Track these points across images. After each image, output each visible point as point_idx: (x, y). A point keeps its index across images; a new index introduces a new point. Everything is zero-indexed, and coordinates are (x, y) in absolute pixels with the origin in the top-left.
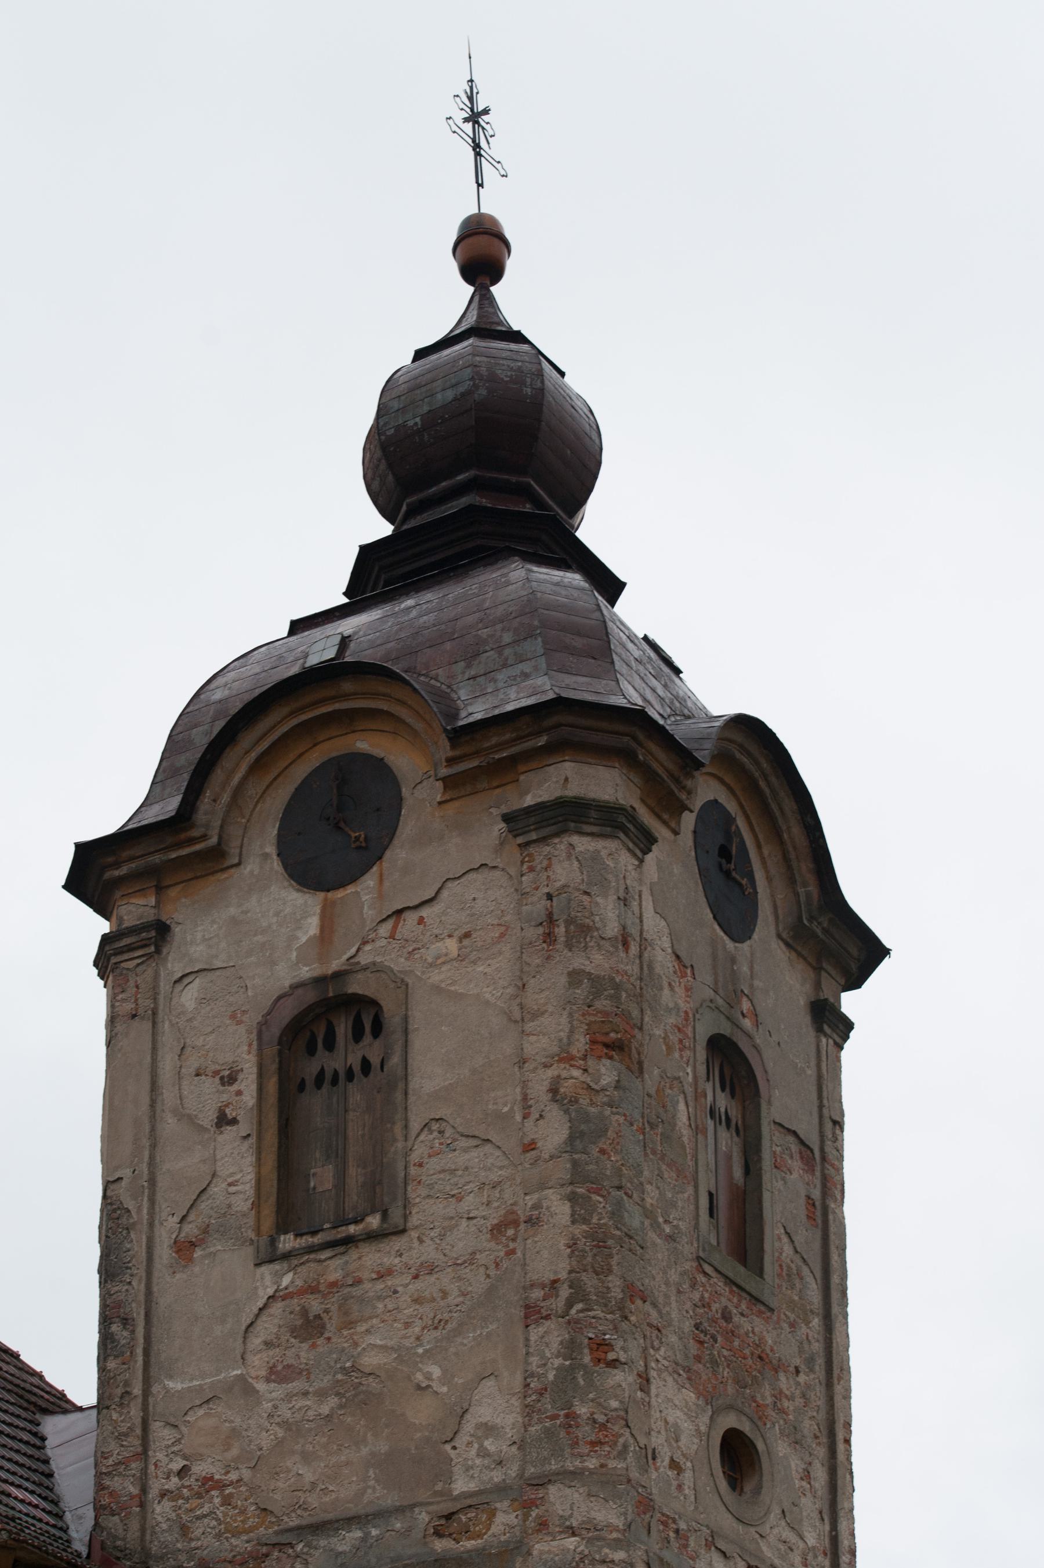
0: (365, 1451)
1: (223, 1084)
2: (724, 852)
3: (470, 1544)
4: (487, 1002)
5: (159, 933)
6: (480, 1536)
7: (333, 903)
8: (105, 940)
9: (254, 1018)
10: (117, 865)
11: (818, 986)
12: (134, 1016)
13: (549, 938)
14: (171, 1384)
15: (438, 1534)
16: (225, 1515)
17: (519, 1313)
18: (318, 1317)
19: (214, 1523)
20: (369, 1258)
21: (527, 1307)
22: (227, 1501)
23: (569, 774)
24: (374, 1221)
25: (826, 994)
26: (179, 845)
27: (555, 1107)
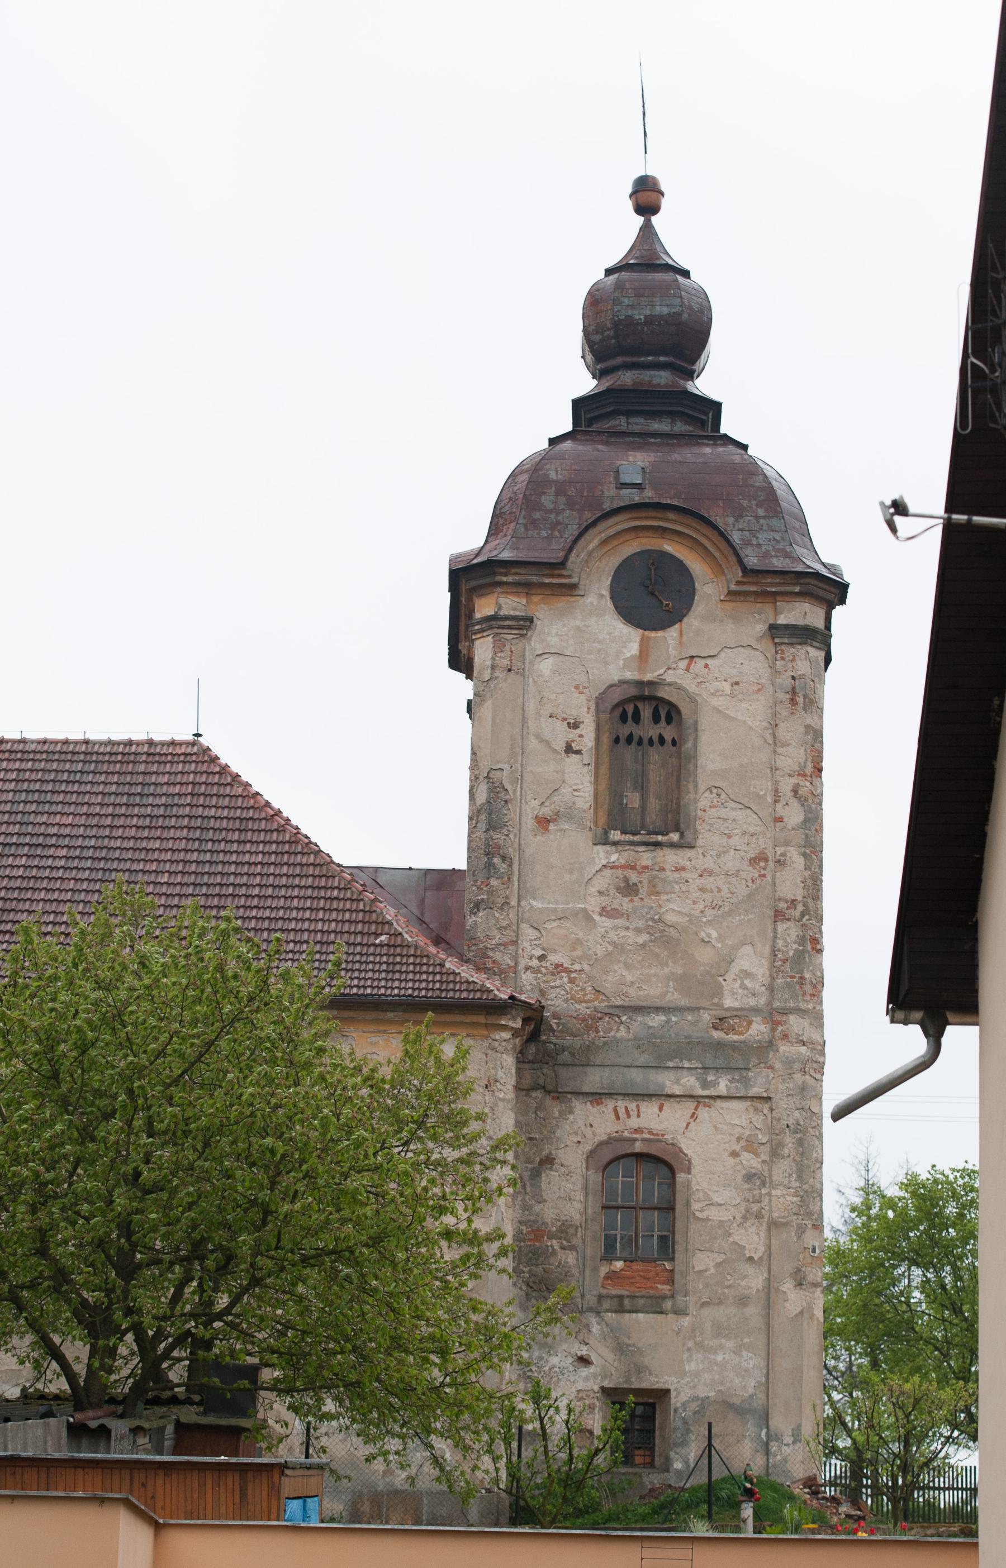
0: (667, 970)
1: (569, 727)
3: (736, 1037)
4: (751, 728)
6: (741, 1033)
7: (649, 639)
10: (506, 574)
12: (510, 670)
13: (793, 701)
14: (534, 903)
15: (715, 1028)
16: (571, 989)
17: (772, 913)
18: (635, 884)
19: (563, 992)
20: (670, 858)
21: (776, 911)
22: (572, 981)
23: (807, 610)
24: (675, 837)
26: (552, 576)
27: (795, 801)
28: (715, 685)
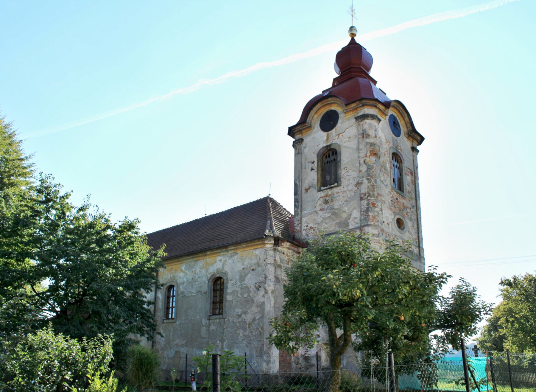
2: (394, 123)
5: (301, 140)
8: (294, 142)
9: (317, 153)
11: (413, 144)
13: (363, 137)
17: (359, 199)
20: (335, 190)
22: (314, 230)
24: (336, 184)
25: (415, 145)
28: (345, 140)
